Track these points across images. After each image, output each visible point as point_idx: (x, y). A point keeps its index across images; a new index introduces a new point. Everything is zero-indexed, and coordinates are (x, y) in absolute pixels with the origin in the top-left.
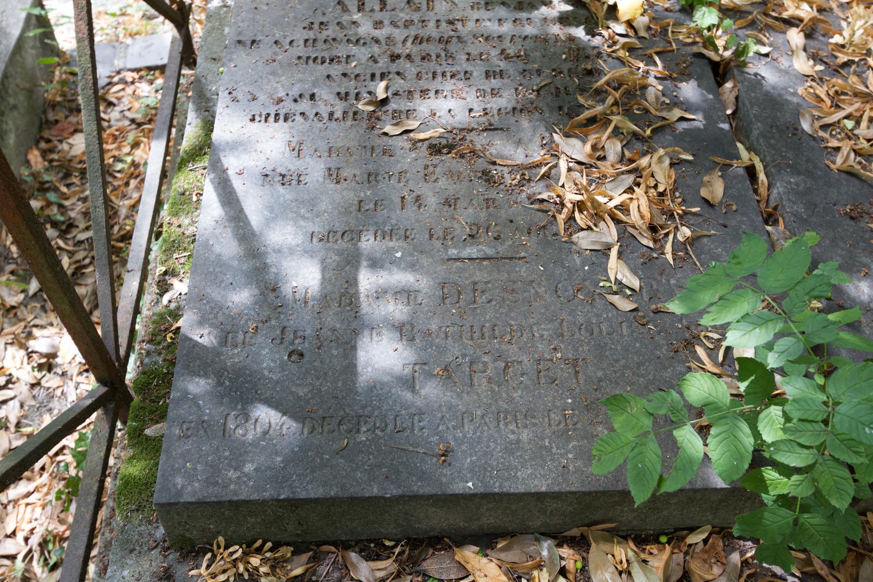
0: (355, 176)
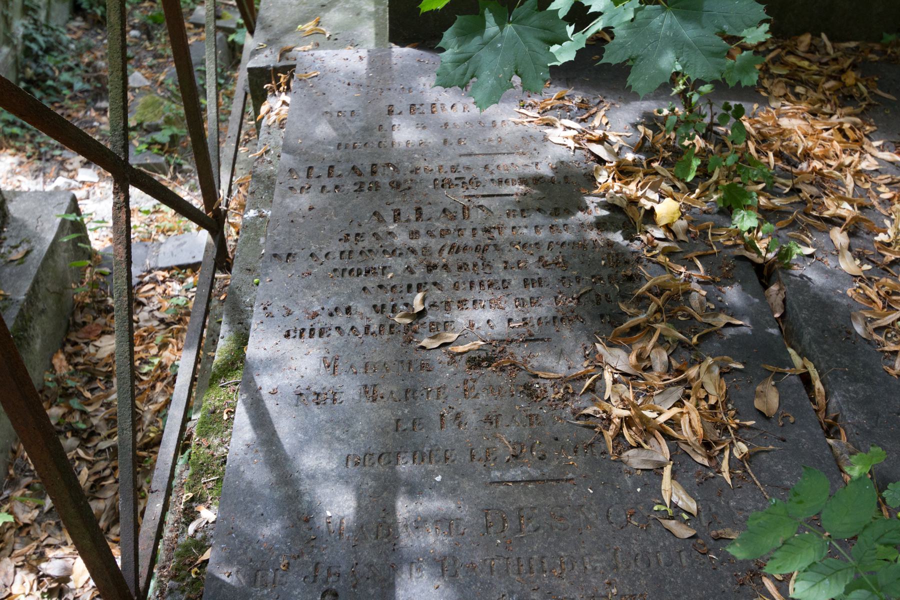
0: (392, 393)
